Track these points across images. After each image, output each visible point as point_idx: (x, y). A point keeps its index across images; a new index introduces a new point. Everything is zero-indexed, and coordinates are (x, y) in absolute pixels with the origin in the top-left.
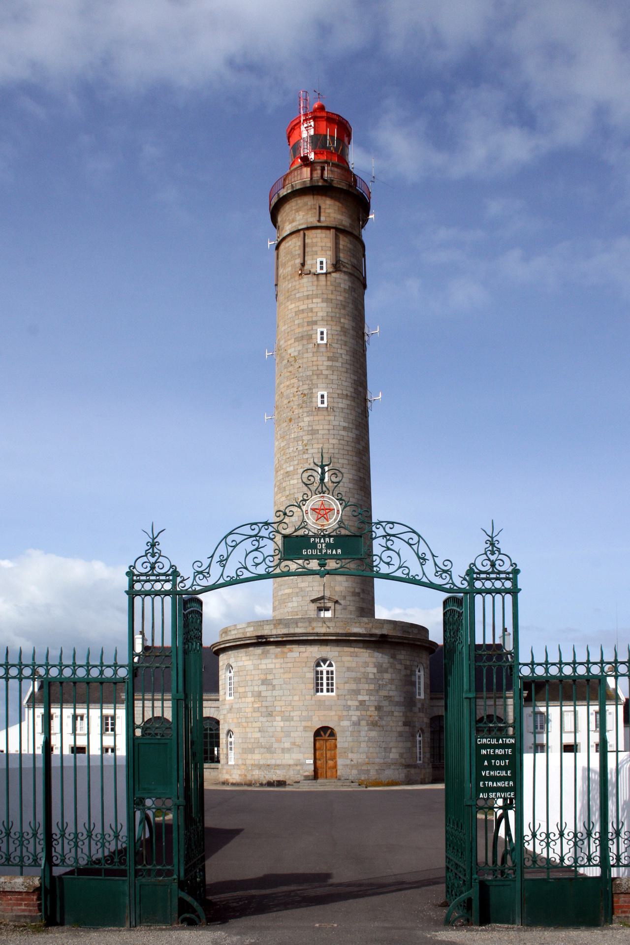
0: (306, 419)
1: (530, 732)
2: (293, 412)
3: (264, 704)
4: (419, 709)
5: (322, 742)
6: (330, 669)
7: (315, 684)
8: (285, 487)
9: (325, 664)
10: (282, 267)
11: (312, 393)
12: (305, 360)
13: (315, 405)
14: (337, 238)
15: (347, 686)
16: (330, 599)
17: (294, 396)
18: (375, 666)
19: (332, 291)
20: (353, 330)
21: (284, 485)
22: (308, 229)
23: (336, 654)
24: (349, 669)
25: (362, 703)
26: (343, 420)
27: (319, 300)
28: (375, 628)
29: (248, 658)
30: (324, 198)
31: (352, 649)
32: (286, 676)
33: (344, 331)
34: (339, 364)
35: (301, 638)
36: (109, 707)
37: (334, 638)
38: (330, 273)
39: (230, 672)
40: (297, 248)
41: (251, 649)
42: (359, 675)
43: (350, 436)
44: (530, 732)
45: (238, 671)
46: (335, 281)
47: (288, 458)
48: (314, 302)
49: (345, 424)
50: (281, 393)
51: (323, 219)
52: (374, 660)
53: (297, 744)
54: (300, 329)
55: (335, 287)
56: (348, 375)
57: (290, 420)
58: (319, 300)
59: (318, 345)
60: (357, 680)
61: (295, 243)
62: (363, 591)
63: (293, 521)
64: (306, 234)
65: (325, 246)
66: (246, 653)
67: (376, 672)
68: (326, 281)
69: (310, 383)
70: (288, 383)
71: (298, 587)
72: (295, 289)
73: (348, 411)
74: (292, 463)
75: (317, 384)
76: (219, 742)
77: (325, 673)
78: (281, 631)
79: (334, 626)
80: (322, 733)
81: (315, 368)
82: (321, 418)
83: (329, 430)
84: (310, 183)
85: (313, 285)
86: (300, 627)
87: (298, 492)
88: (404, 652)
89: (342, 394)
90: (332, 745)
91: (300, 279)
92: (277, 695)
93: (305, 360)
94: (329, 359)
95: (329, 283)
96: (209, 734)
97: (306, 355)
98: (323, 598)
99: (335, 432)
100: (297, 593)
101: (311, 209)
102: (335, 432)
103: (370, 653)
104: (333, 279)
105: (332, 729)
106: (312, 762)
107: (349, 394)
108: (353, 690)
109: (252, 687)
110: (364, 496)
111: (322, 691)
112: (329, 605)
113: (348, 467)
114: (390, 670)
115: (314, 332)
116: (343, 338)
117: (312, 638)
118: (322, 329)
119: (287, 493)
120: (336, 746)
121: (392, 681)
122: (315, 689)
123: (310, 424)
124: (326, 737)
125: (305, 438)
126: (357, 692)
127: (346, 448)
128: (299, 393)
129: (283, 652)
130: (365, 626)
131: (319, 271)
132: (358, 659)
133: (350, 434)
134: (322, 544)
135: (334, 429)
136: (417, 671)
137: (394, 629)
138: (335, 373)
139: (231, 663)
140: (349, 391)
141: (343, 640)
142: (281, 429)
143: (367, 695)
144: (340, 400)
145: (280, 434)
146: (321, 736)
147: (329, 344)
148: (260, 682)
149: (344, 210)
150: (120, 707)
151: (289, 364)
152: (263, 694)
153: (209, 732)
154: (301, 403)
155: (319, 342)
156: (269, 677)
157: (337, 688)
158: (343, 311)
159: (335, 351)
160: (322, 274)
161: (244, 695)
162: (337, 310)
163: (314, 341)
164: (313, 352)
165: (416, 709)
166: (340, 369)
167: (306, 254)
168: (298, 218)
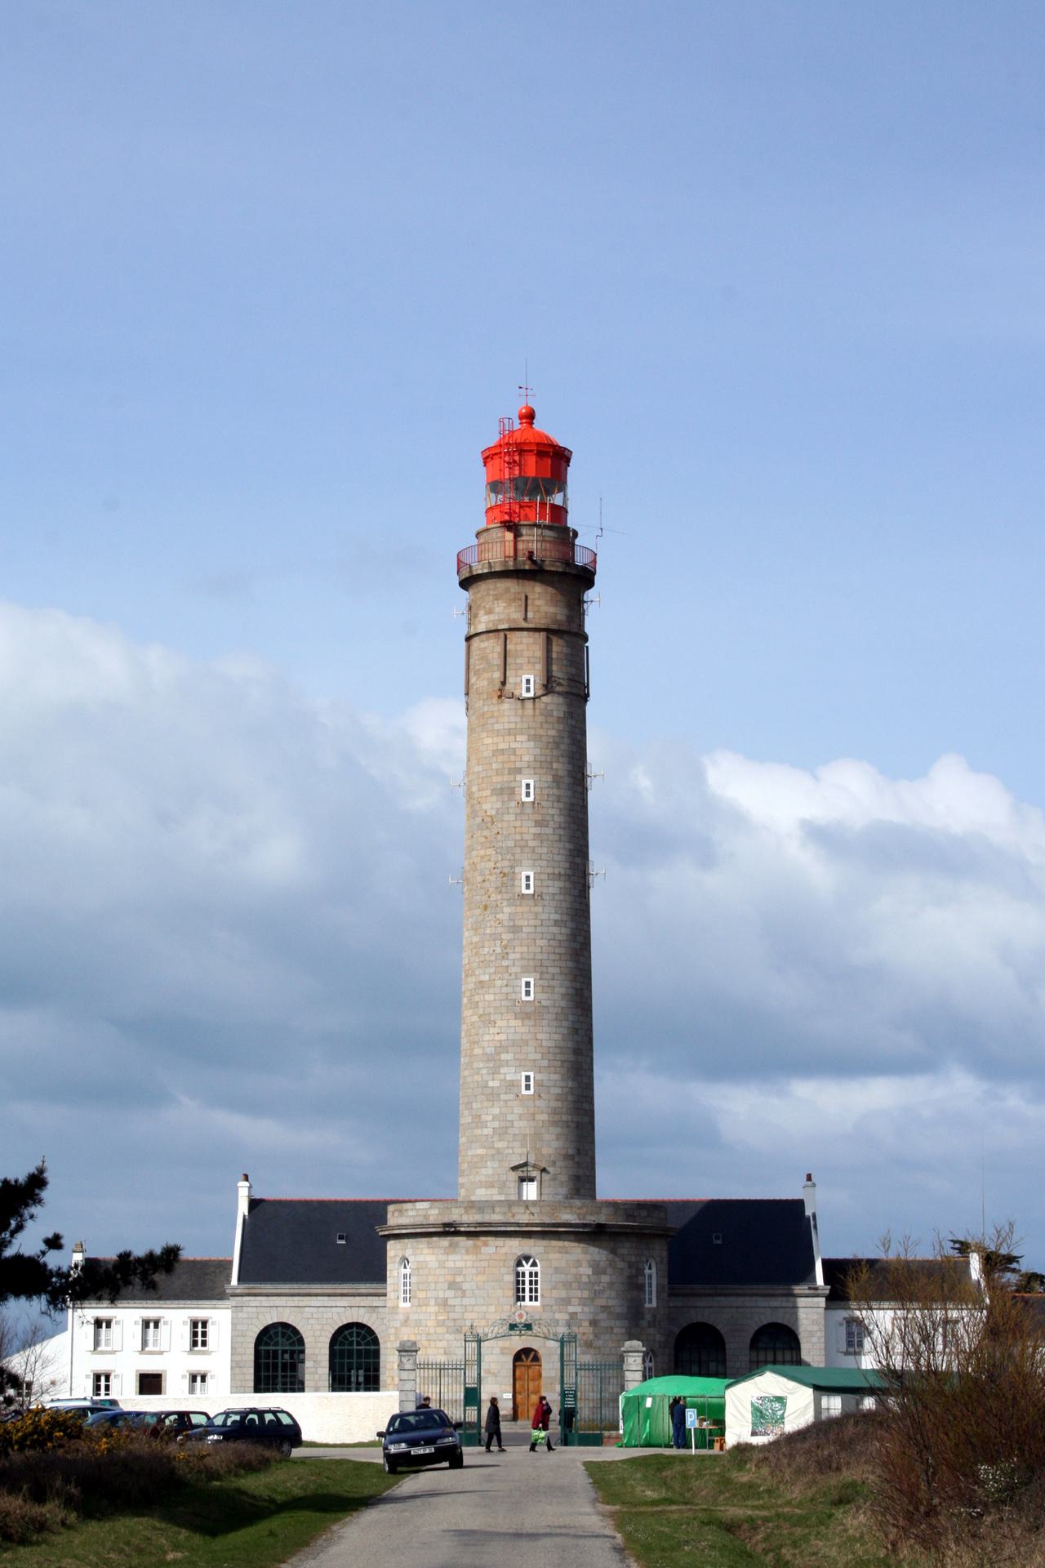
0: (507, 910)
1: (842, 1352)
2: (489, 897)
3: (452, 1316)
4: (649, 1322)
5: (523, 1369)
6: (534, 1269)
7: (515, 1291)
8: (477, 1002)
9: (527, 1263)
10: (475, 675)
11: (514, 873)
12: (505, 825)
13: (517, 890)
14: (549, 642)
15: (555, 1293)
16: (535, 1166)
17: (491, 874)
18: (590, 1266)
19: (541, 723)
20: (568, 737)
21: (477, 998)
22: (510, 630)
23: (541, 1250)
24: (557, 1270)
25: (573, 1315)
26: (553, 912)
27: (523, 738)
28: (591, 1214)
29: (431, 1251)
30: (532, 583)
31: (560, 1243)
32: (480, 1278)
33: (557, 780)
34: (549, 831)
35: (499, 1229)
36: (200, 1306)
37: (539, 1229)
38: (539, 697)
39: (405, 1267)
40: (496, 655)
41: (435, 1239)
42: (569, 1278)
43: (561, 932)
44: (842, 1352)
45: (418, 1269)
46: (546, 708)
47: (483, 962)
48: (517, 740)
49: (557, 917)
50: (474, 863)
51: (530, 615)
52: (588, 1257)
53: (492, 1371)
54: (499, 777)
55: (546, 716)
56: (562, 845)
57: (486, 907)
58: (523, 738)
59: (523, 803)
60: (567, 1285)
61: (493, 647)
62: (579, 1152)
63: (489, 1053)
64: (508, 636)
65: (534, 657)
66: (428, 1243)
67: (591, 1273)
68: (534, 709)
69: (512, 858)
70: (482, 853)
71: (494, 1148)
72: (492, 717)
73: (562, 897)
74: (487, 970)
75: (521, 860)
76: (378, 1363)
77: (527, 1275)
78: (473, 1217)
79: (539, 1211)
80: (523, 1356)
81: (518, 837)
82: (525, 909)
83: (535, 926)
84: (514, 566)
85: (516, 715)
86: (497, 1213)
87: (495, 1013)
88: (627, 1245)
89: (554, 874)
90: (536, 1373)
91: (498, 703)
92: (468, 1304)
93: (505, 825)
94: (538, 824)
95: (537, 712)
96: (355, 1351)
97: (506, 817)
98: (525, 1164)
99: (544, 929)
100: (493, 1156)
101: (514, 600)
102: (544, 929)
103: (583, 1247)
104: (543, 706)
105: (536, 1351)
106: (510, 1396)
107: (562, 872)
108: (563, 1299)
109: (436, 1292)
110: (582, 1015)
112: (535, 1173)
113: (559, 977)
114: (609, 1270)
115: (518, 784)
116: (555, 791)
117: (512, 1229)
118: (528, 781)
120: (540, 1375)
121: (611, 1284)
122: (515, 1297)
123: (512, 917)
124: (529, 1363)
125: (504, 936)
126: (567, 1301)
127: (557, 951)
128: (498, 871)
129: (475, 1246)
130: (578, 1211)
131: (525, 695)
132: (568, 1257)
133: (564, 930)
134: (520, 1326)
135: (542, 925)
136: (647, 1268)
137: (615, 1213)
138: (545, 844)
139: (407, 1256)
140: (562, 867)
141: (549, 1232)
142: (472, 916)
143: (579, 1305)
144: (550, 883)
145: (472, 924)
146: (521, 1360)
147: (536, 802)
148: (446, 1286)
149: (559, 597)
150: (217, 1306)
151: (483, 825)
152: (450, 1302)
153: (355, 1347)
154: (500, 885)
155: (524, 799)
156: (459, 1279)
157: (542, 1296)
158: (555, 752)
159: (545, 811)
160: (529, 699)
161: (424, 1303)
162: (547, 751)
163: (517, 797)
164: (516, 814)
165: (644, 1323)
166: (551, 838)
167: (508, 668)
168: (497, 610)
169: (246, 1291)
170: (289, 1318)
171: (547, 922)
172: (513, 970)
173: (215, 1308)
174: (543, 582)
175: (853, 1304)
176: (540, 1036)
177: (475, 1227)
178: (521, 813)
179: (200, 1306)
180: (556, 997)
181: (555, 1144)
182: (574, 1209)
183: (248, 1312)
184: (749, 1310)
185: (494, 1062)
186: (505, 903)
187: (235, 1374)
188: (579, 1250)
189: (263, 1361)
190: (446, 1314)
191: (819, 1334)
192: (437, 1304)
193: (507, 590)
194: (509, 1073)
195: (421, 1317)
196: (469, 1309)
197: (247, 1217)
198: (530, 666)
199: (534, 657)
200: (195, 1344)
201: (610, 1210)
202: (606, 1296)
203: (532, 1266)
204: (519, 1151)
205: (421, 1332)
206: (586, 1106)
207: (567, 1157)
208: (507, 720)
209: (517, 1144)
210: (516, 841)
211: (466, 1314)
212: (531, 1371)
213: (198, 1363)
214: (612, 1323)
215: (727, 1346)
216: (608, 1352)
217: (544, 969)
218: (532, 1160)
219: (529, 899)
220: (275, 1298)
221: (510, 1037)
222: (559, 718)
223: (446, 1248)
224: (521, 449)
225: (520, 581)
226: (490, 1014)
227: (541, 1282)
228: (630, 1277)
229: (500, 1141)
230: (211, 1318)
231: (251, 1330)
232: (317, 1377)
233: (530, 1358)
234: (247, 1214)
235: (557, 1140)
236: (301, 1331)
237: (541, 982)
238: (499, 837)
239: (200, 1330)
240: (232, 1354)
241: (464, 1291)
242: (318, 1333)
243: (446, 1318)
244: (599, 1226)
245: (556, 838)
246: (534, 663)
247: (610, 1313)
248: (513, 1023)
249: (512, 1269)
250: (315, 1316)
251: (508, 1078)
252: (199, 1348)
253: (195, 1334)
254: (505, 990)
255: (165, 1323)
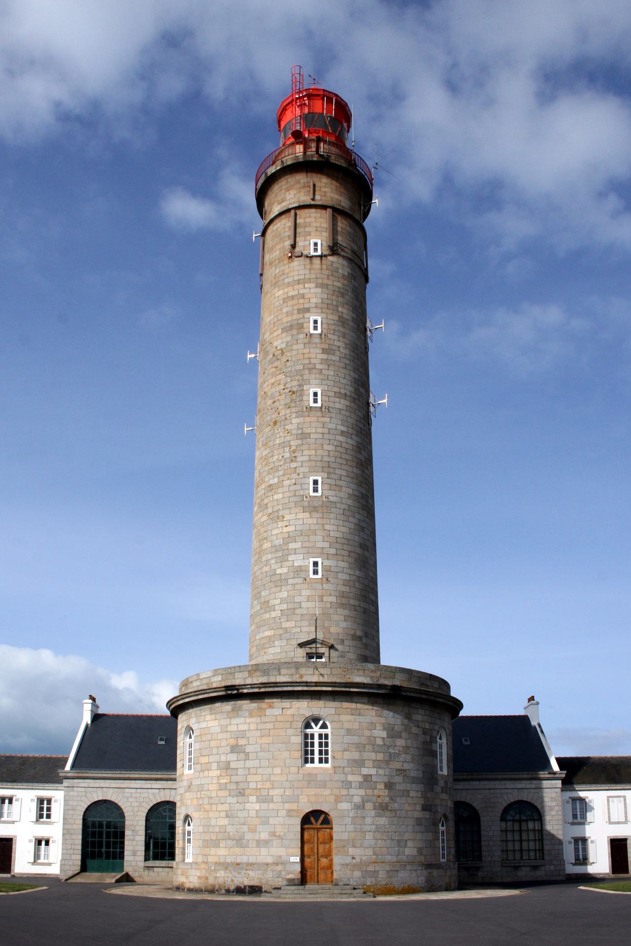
0: (295, 421)
3: (234, 779)
5: (312, 832)
6: (324, 731)
7: (303, 753)
8: (267, 504)
9: (316, 725)
11: (303, 390)
12: (294, 353)
15: (347, 755)
17: (280, 395)
18: (384, 729)
19: (328, 276)
21: (266, 501)
24: (349, 732)
25: (367, 778)
28: (385, 678)
29: (213, 717)
30: (319, 176)
32: (265, 740)
33: (342, 321)
35: (285, 689)
36: (34, 787)
37: (330, 689)
38: (325, 256)
39: (190, 737)
42: (363, 740)
46: (332, 265)
47: (272, 468)
48: (306, 287)
51: (317, 197)
52: (383, 720)
57: (275, 423)
58: (312, 285)
59: (311, 335)
60: (360, 747)
62: (366, 635)
66: (211, 709)
67: (385, 736)
73: (348, 414)
74: (276, 474)
79: (329, 673)
80: (312, 819)
81: (307, 361)
82: (314, 419)
83: (323, 434)
88: (421, 711)
90: (327, 837)
94: (324, 351)
95: (324, 267)
98: (314, 641)
100: (280, 635)
101: (304, 187)
102: (331, 437)
105: (326, 814)
106: (298, 859)
107: (348, 394)
108: (355, 761)
111: (312, 761)
112: (323, 650)
114: (404, 735)
115: (307, 320)
119: (270, 510)
120: (331, 838)
125: (292, 443)
126: (360, 763)
127: (344, 456)
128: (287, 391)
129: (260, 709)
130: (371, 675)
131: (312, 253)
132: (361, 719)
138: (332, 368)
139: (191, 725)
140: (349, 390)
143: (374, 767)
144: (338, 400)
147: (323, 334)
148: (229, 749)
150: (58, 788)
152: (233, 765)
154: (289, 402)
155: (312, 331)
156: (241, 742)
157: (333, 757)
158: (340, 299)
159: (332, 342)
160: (317, 256)
161: (206, 768)
165: (438, 789)
167: (297, 235)
169: (76, 775)
170: (120, 801)
171: (334, 431)
172: (301, 470)
173: (57, 790)
174: (328, 176)
175: (577, 787)
176: (327, 527)
177: (259, 688)
178: (309, 343)
179: (34, 787)
180: (342, 495)
181: (344, 624)
182: (367, 672)
183: (78, 792)
184: (498, 791)
185: (282, 552)
186: (294, 415)
187: (66, 839)
188: (373, 713)
189: (90, 829)
190: (229, 777)
191: (557, 808)
192: (219, 768)
193: (298, 182)
194: (298, 561)
195: (203, 781)
196: (253, 771)
197: (89, 725)
198: (318, 233)
199: (321, 227)
200: (41, 816)
201: (405, 676)
202: (401, 759)
203: (321, 728)
204: (305, 629)
205: (203, 796)
206: (372, 608)
207: (355, 637)
208: (296, 273)
209: (305, 623)
210: (304, 365)
211: (249, 776)
212: (321, 834)
213: (42, 831)
214: (409, 786)
215: (482, 819)
216: (404, 815)
217: (332, 470)
218: (320, 636)
219: (317, 411)
220: (101, 781)
221: (299, 528)
222: (343, 275)
223: (228, 712)
224: (312, 95)
225: (309, 174)
226: (278, 511)
227: (332, 743)
228: (424, 743)
229: (287, 621)
230: (54, 797)
231: (80, 805)
232: (135, 843)
233: (320, 821)
234: (89, 722)
235: (345, 621)
236: (122, 807)
237: (328, 481)
238: (288, 364)
239: (45, 806)
240: (64, 824)
241: (247, 754)
242: (136, 809)
243: (228, 781)
244: (394, 687)
245: (342, 365)
246: (322, 231)
247: (405, 776)
248: (301, 515)
249: (300, 730)
250: (133, 795)
251: (296, 564)
252: (45, 819)
253: (42, 809)
254: (293, 488)
255: (17, 800)
